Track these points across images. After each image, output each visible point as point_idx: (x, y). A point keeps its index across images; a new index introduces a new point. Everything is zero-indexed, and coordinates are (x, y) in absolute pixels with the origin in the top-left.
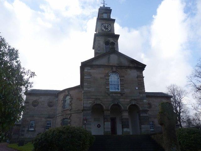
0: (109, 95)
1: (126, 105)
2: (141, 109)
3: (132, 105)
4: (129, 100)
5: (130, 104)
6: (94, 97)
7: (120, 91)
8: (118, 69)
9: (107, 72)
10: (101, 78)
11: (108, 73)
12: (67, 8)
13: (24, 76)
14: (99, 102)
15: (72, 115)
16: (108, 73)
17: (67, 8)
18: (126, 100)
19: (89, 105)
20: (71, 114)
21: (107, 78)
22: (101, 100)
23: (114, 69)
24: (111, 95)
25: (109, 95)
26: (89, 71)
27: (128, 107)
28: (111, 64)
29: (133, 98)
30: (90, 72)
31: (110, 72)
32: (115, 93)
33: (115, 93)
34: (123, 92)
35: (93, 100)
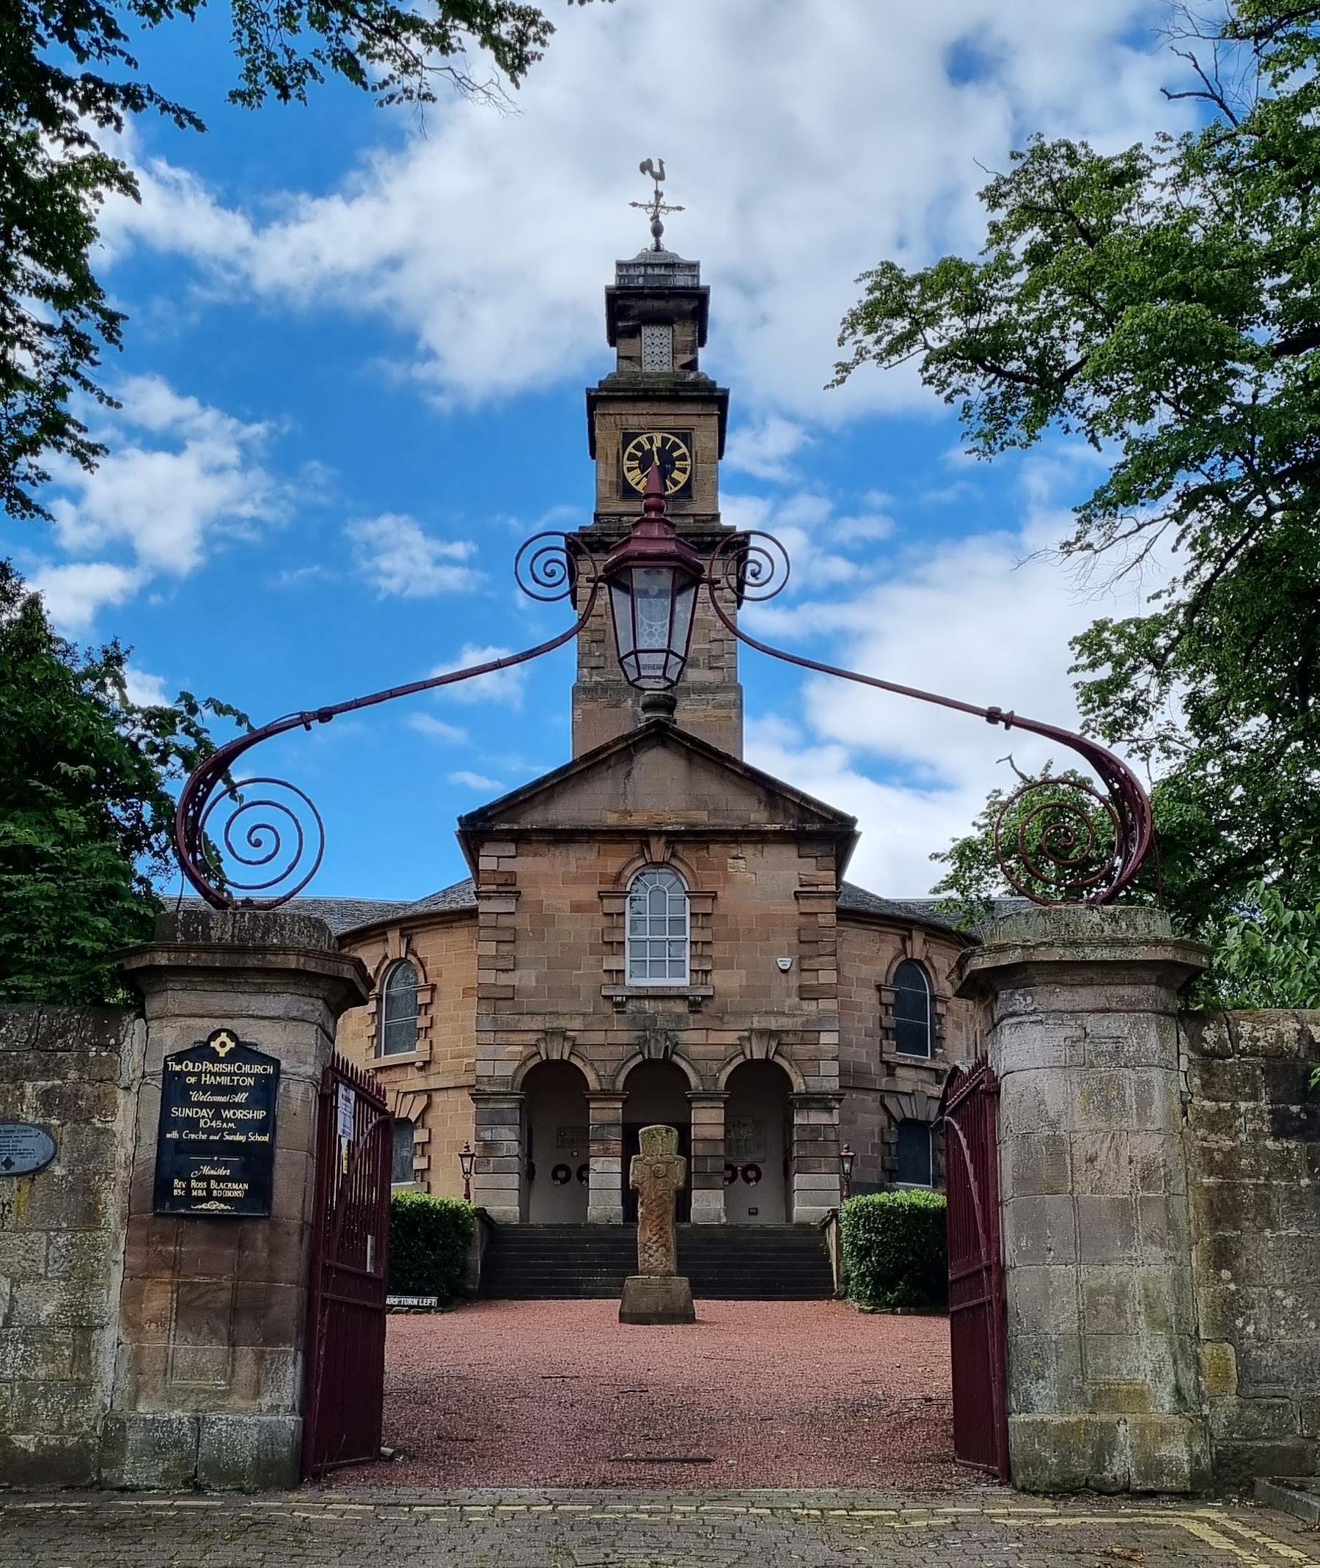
0: (619, 1006)
1: (715, 1066)
2: (799, 1085)
3: (750, 1065)
4: (731, 1038)
5: (740, 1059)
6: (537, 1023)
7: (685, 982)
8: (679, 848)
9: (613, 866)
10: (577, 908)
11: (617, 878)
12: (144, 26)
13: (990, 896)
14: (557, 1051)
15: (437, 1098)
16: (617, 878)
17: (144, 26)
18: (714, 1037)
19: (508, 1069)
20: (429, 1093)
21: (612, 905)
22: (574, 1039)
23: (658, 850)
24: (631, 1006)
25: (619, 1006)
26: (507, 865)
27: (723, 1078)
28: (638, 821)
29: (757, 1023)
30: (513, 873)
31: (627, 873)
32: (655, 998)
33: (655, 998)
34: (703, 992)
35: (532, 1038)
